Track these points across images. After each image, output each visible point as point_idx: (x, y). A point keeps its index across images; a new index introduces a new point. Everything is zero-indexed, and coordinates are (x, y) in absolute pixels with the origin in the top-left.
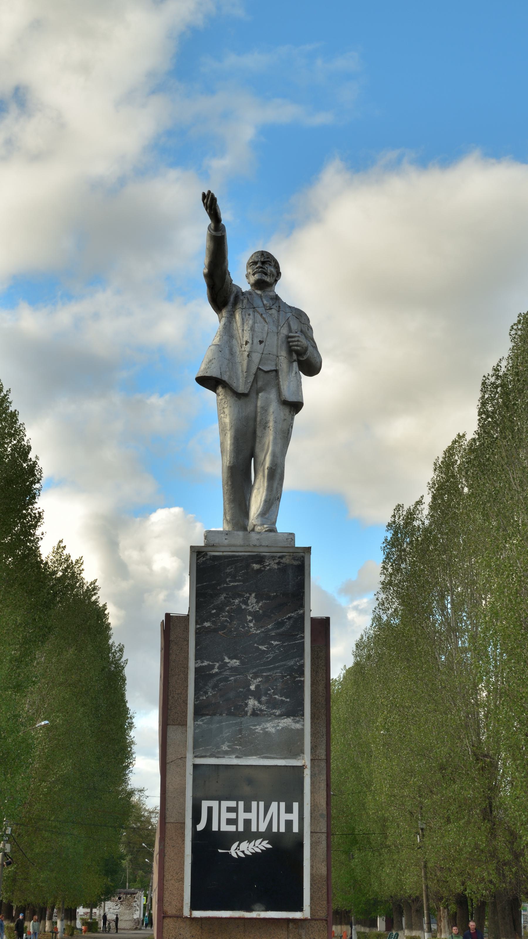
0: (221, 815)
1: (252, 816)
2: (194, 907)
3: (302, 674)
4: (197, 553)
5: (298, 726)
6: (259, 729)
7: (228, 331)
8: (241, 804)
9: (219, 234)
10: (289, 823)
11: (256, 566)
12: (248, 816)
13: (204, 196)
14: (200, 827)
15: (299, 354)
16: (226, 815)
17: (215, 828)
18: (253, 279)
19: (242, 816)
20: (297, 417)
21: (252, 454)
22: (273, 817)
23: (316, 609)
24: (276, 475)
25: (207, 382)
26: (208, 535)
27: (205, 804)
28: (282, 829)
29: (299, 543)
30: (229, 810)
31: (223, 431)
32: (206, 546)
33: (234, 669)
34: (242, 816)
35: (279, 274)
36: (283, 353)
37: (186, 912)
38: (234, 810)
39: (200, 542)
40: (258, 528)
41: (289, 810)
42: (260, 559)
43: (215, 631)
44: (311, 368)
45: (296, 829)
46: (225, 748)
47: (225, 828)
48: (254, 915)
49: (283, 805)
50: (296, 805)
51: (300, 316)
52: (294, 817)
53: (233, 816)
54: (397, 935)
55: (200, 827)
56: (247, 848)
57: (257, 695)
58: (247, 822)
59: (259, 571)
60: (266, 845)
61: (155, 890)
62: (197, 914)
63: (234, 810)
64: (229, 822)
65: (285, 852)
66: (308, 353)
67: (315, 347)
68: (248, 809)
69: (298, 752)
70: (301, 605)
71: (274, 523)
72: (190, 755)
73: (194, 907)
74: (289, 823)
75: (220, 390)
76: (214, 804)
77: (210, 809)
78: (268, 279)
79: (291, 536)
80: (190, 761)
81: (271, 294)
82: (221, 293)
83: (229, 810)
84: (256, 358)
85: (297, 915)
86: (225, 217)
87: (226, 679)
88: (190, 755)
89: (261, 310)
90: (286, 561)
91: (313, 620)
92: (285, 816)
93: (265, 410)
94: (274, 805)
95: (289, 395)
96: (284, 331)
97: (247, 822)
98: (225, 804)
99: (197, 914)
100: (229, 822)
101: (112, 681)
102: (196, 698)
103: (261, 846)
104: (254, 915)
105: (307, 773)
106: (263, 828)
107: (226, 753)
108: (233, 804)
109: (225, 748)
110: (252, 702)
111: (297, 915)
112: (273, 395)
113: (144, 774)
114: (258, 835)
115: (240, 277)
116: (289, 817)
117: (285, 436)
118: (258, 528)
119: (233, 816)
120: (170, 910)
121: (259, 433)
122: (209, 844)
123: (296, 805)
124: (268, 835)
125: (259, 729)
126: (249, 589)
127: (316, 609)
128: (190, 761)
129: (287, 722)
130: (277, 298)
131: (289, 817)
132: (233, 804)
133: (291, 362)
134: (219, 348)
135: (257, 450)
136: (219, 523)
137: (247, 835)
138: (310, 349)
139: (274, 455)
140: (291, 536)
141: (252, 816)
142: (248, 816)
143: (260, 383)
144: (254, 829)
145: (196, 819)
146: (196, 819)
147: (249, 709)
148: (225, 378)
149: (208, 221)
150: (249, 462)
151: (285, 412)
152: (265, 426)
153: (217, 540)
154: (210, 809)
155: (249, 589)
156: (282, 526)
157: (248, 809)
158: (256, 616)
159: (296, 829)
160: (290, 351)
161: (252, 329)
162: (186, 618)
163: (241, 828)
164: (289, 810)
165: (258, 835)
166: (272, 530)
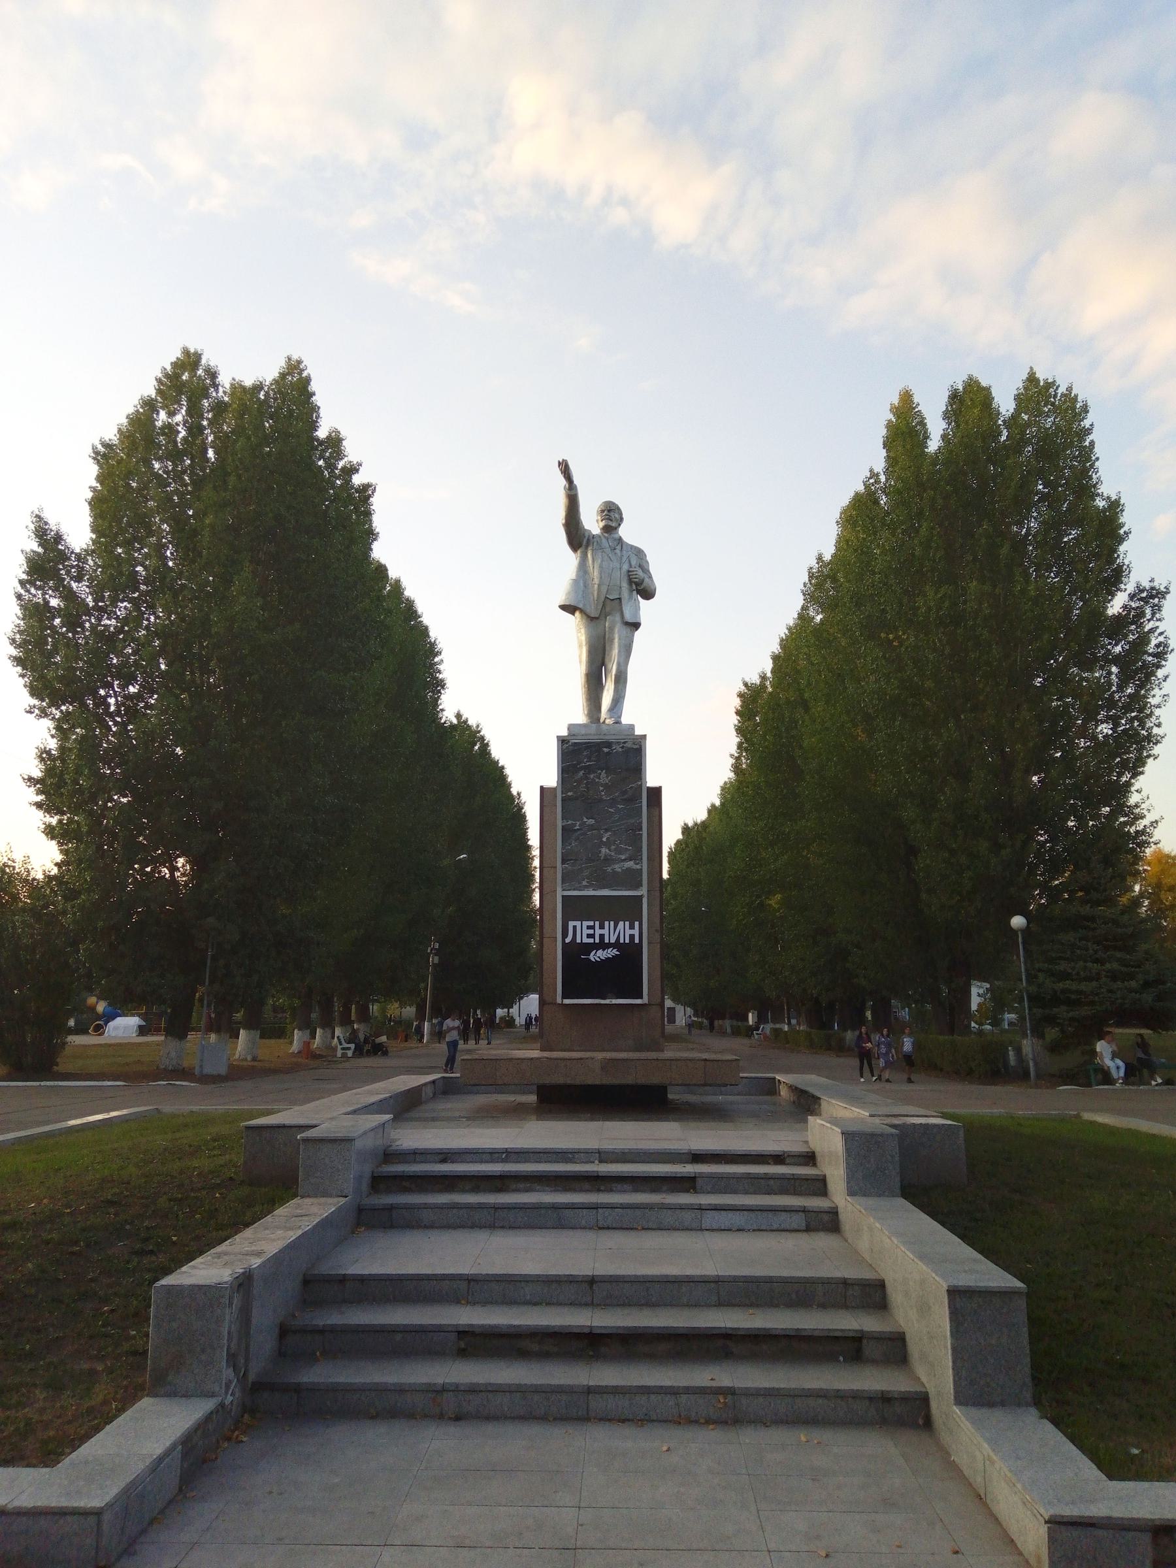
0: (582, 931)
1: (605, 932)
2: (564, 997)
3: (641, 829)
4: (562, 741)
5: (638, 867)
6: (609, 869)
7: (582, 567)
8: (597, 923)
9: (573, 493)
10: (632, 937)
11: (606, 750)
12: (602, 931)
13: (559, 463)
14: (568, 940)
15: (637, 584)
16: (586, 932)
17: (579, 941)
18: (602, 524)
19: (598, 932)
20: (637, 633)
21: (603, 664)
22: (622, 931)
23: (651, 781)
24: (621, 680)
25: (569, 608)
26: (570, 727)
27: (571, 924)
28: (627, 941)
29: (638, 732)
30: (589, 927)
31: (580, 646)
32: (569, 735)
33: (592, 828)
34: (598, 932)
35: (622, 519)
36: (625, 585)
37: (559, 1000)
38: (593, 927)
39: (565, 733)
40: (607, 721)
41: (632, 927)
42: (608, 744)
43: (576, 798)
44: (648, 594)
45: (637, 941)
46: (584, 883)
47: (586, 940)
48: (607, 1001)
49: (627, 923)
50: (637, 924)
51: (639, 553)
52: (636, 932)
53: (591, 932)
54: (1171, 889)
55: (568, 940)
56: (601, 954)
57: (608, 844)
58: (602, 936)
59: (608, 753)
60: (615, 952)
61: (371, 1093)
62: (567, 1001)
63: (593, 927)
64: (589, 936)
65: (629, 953)
66: (645, 584)
67: (650, 577)
68: (602, 927)
69: (639, 885)
70: (640, 779)
71: (620, 717)
72: (559, 889)
73: (564, 997)
74: (632, 937)
75: (577, 614)
76: (578, 924)
77: (575, 927)
78: (614, 525)
79: (632, 727)
80: (560, 893)
81: (616, 536)
82: (576, 536)
83: (589, 927)
84: (604, 589)
85: (638, 1001)
86: (576, 481)
87: (585, 834)
88: (559, 889)
89: (608, 550)
90: (629, 745)
91: (649, 788)
92: (629, 932)
93: (612, 629)
94: (621, 924)
95: (628, 617)
96: (625, 567)
97: (602, 936)
98: (586, 924)
99: (567, 1001)
100: (589, 936)
101: (520, 818)
102: (563, 848)
103: (611, 953)
104: (607, 1001)
105: (645, 901)
106: (613, 941)
107: (586, 887)
108: (591, 923)
109: (584, 883)
110: (604, 850)
111: (638, 1001)
112: (618, 618)
113: (207, 1271)
114: (609, 945)
115: (591, 523)
116: (632, 932)
117: (627, 650)
118: (607, 721)
119: (591, 932)
120: (548, 999)
121: (607, 648)
122: (575, 953)
123: (637, 924)
124: (617, 945)
125: (609, 869)
126: (603, 766)
127: (651, 781)
128: (560, 893)
129: (630, 864)
130: (620, 539)
131: (632, 932)
132: (591, 923)
133: (631, 591)
134: (575, 582)
135: (607, 660)
136: (579, 716)
137: (603, 945)
138: (647, 580)
139: (619, 664)
140: (632, 727)
141: (605, 932)
142: (602, 931)
143: (608, 609)
144: (607, 941)
145: (565, 935)
146: (565, 935)
147: (602, 855)
148: (581, 606)
149: (563, 482)
150: (602, 667)
151: (626, 631)
152: (612, 640)
153: (576, 731)
154: (575, 927)
155: (603, 766)
156: (625, 720)
157: (602, 927)
158: (606, 786)
159: (637, 941)
160: (630, 582)
161: (601, 567)
162: (555, 789)
163: (597, 941)
164: (632, 927)
165: (609, 945)
166: (618, 722)
